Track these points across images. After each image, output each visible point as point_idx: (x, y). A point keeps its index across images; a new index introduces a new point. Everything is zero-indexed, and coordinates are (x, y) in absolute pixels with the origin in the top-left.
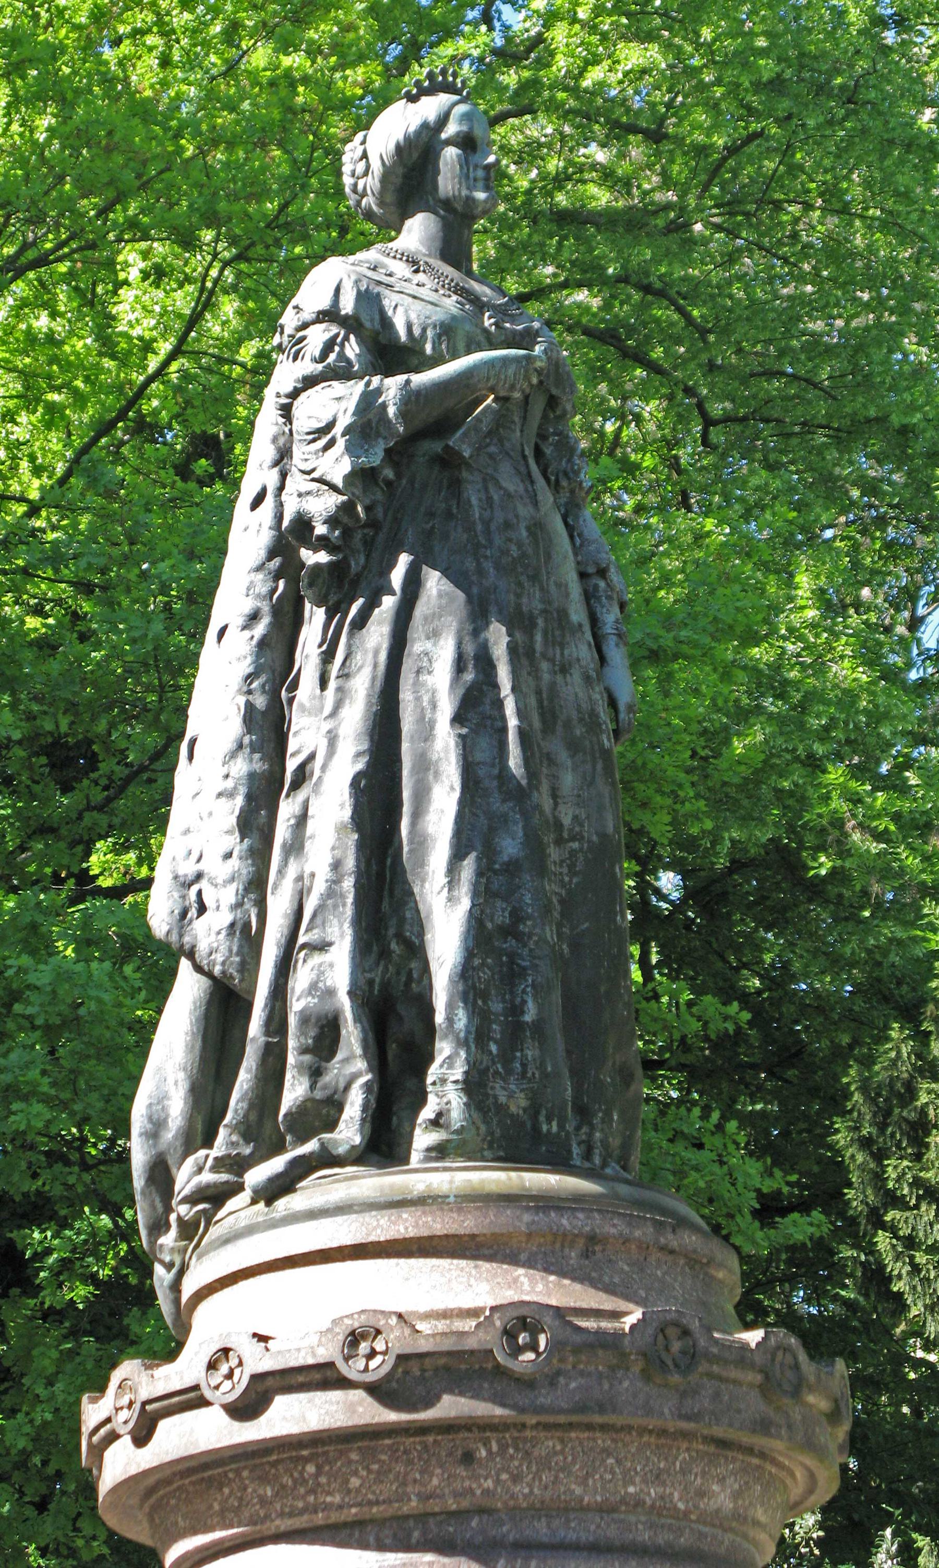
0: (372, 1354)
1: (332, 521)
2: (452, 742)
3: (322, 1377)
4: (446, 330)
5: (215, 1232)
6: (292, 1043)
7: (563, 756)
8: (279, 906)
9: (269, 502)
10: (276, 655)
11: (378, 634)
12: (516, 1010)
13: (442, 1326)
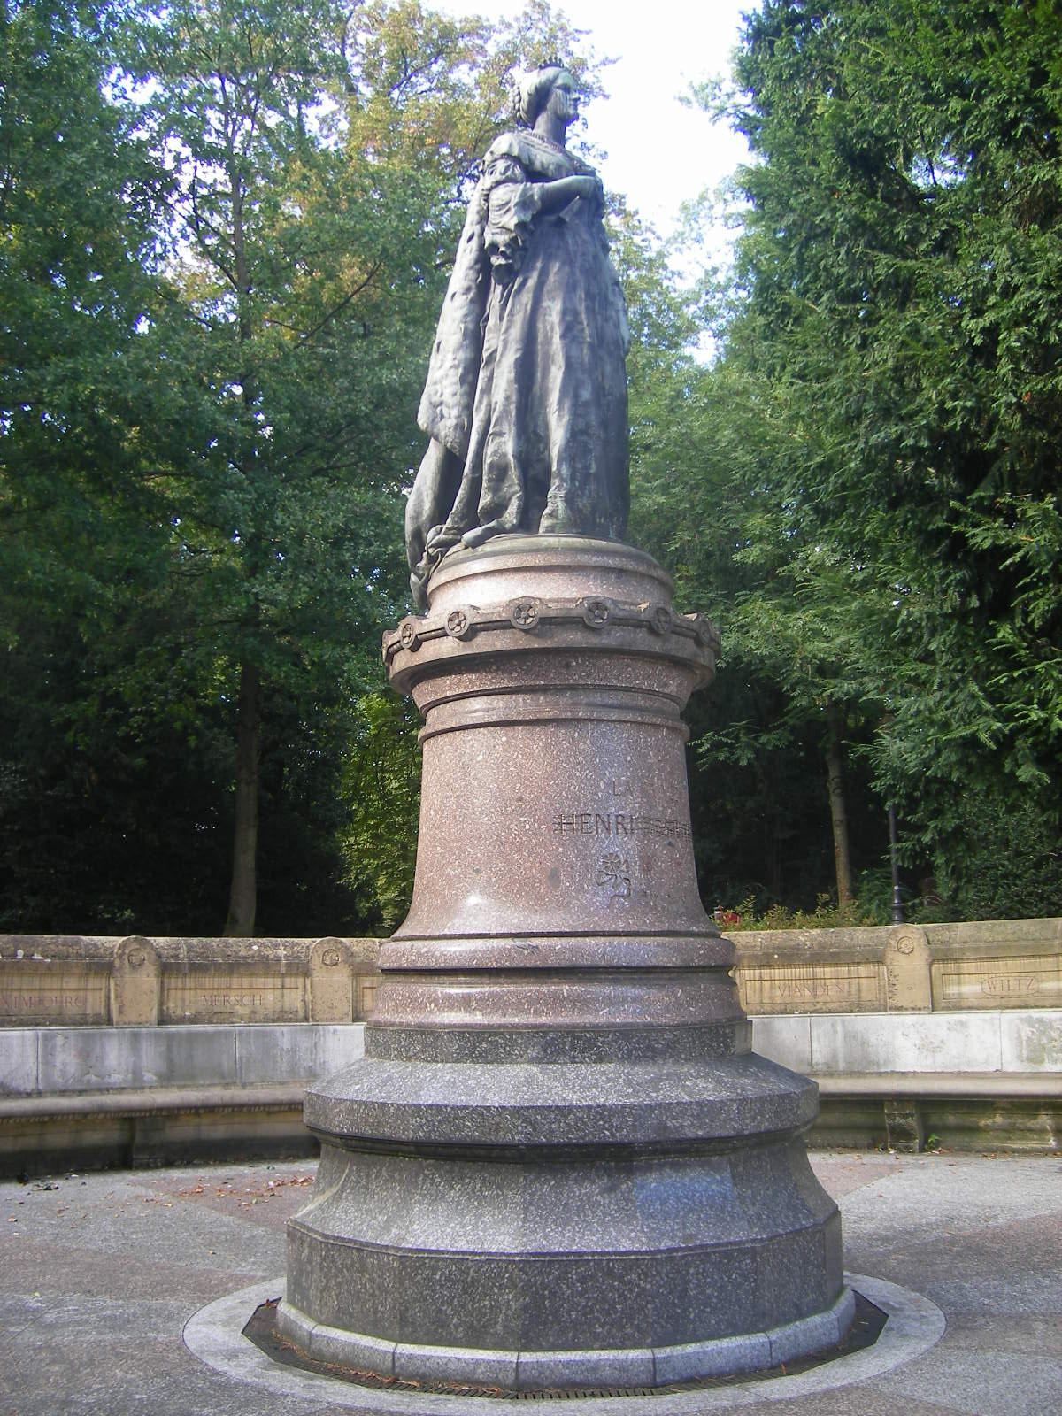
0: (527, 618)
1: (507, 245)
2: (560, 347)
3: (503, 625)
4: (559, 167)
5: (445, 561)
6: (485, 478)
7: (606, 358)
8: (478, 419)
9: (475, 239)
10: (477, 308)
11: (527, 297)
12: (587, 468)
13: (560, 605)
